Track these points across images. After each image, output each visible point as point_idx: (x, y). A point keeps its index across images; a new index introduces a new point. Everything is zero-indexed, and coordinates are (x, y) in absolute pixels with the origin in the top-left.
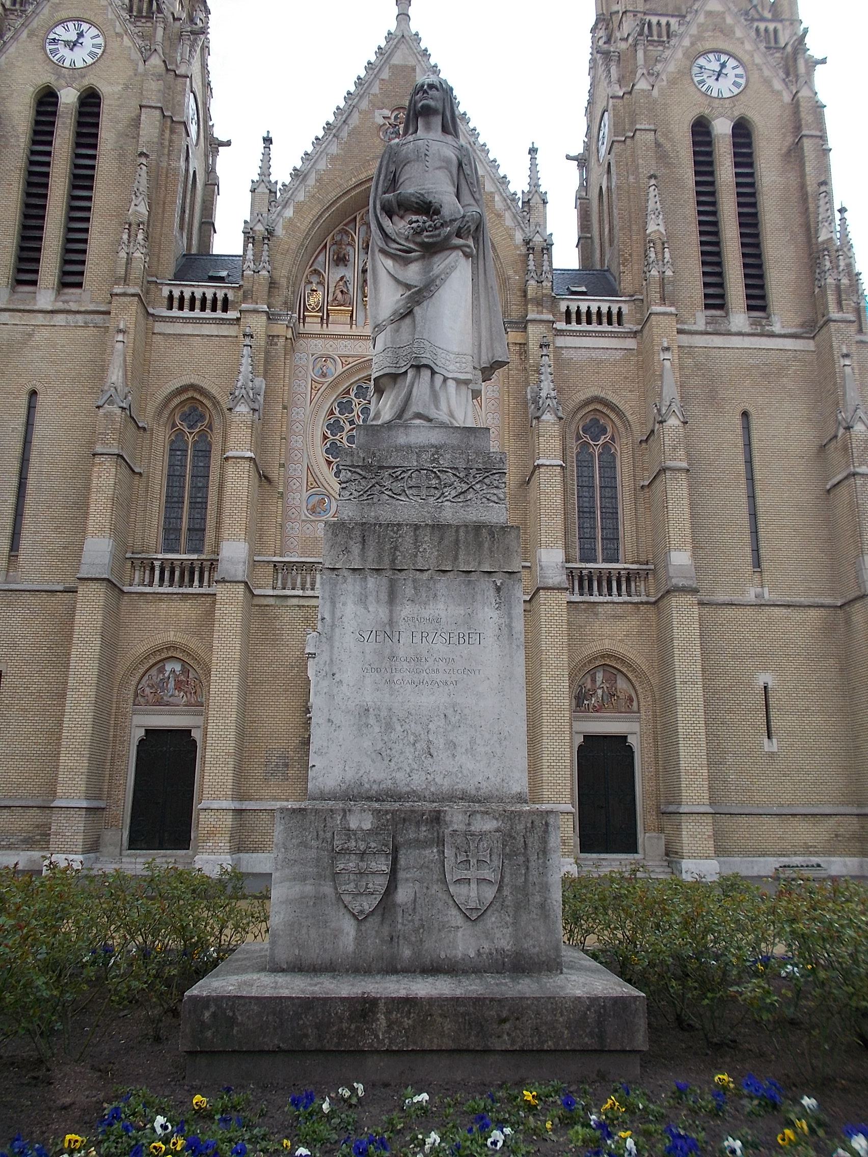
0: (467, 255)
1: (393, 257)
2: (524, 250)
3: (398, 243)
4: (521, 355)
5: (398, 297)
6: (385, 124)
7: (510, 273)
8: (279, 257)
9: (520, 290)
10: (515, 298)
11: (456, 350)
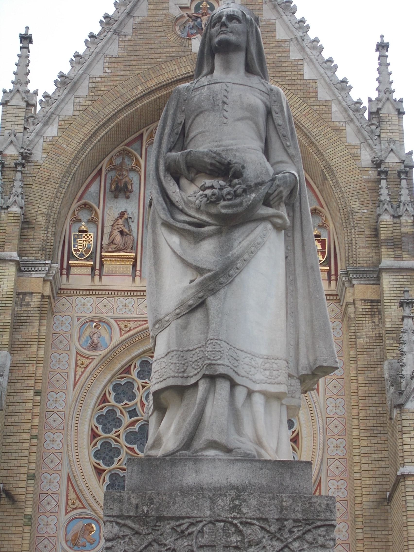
0: (278, 228)
1: (181, 232)
2: (373, 174)
3: (187, 214)
4: (372, 316)
5: (186, 283)
6: (182, 17)
7: (355, 205)
8: (35, 187)
9: (369, 228)
10: (362, 239)
11: (264, 352)
